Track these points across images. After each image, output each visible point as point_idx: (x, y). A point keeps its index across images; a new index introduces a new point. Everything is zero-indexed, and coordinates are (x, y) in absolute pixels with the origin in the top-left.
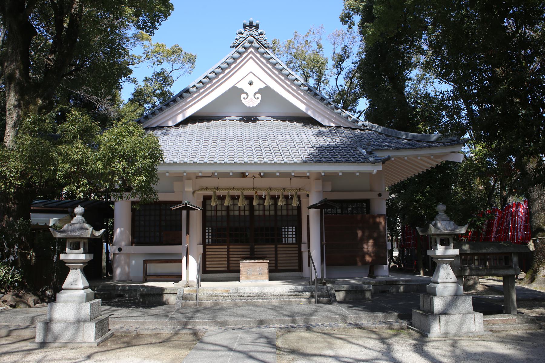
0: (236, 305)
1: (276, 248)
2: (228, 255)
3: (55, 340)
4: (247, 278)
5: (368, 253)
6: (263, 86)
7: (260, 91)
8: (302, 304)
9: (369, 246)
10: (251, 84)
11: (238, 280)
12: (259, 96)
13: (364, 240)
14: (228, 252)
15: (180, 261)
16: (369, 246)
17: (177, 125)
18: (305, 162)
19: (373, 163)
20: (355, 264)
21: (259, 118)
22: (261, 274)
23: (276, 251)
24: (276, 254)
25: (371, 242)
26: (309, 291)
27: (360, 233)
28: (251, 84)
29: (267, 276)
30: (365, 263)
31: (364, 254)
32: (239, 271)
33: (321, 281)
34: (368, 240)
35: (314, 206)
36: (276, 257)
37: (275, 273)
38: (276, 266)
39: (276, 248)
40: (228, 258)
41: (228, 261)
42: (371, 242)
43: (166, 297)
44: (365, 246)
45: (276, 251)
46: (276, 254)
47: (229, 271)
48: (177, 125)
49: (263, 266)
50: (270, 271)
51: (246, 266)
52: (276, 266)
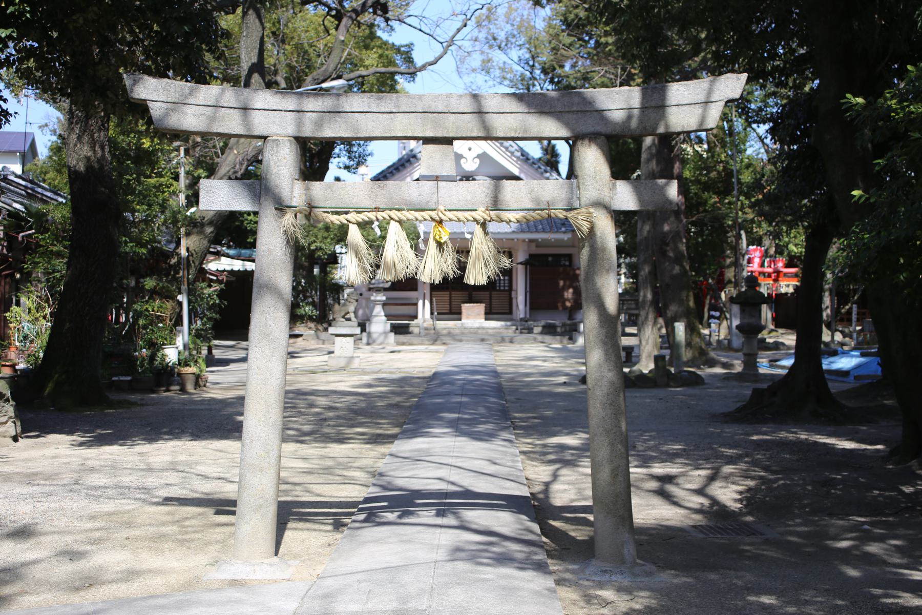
0: (463, 333)
1: (490, 294)
2: (450, 299)
3: (374, 341)
4: (468, 318)
5: (568, 300)
6: (481, 152)
7: (479, 156)
8: (511, 332)
9: (569, 294)
10: (470, 149)
11: (460, 320)
12: (477, 161)
13: (565, 288)
14: (450, 297)
15: (416, 304)
16: (569, 294)
17: (262, 39)
18: (514, 232)
19: (564, 232)
20: (556, 308)
21: (476, 178)
22: (479, 315)
23: (491, 297)
24: (491, 299)
25: (571, 290)
26: (648, 590)
27: (561, 283)
28: (470, 149)
29: (483, 316)
30: (565, 308)
31: (565, 300)
32: (460, 313)
33: (524, 320)
34: (569, 288)
35: (521, 263)
36: (491, 302)
37: (490, 314)
38: (490, 309)
39: (490, 294)
40: (450, 302)
41: (450, 305)
42: (571, 290)
43: (411, 329)
44: (566, 294)
45: (491, 297)
46: (491, 299)
47: (451, 313)
48: (262, 39)
49: (480, 308)
50: (486, 313)
51: (466, 307)
52: (490, 309)
